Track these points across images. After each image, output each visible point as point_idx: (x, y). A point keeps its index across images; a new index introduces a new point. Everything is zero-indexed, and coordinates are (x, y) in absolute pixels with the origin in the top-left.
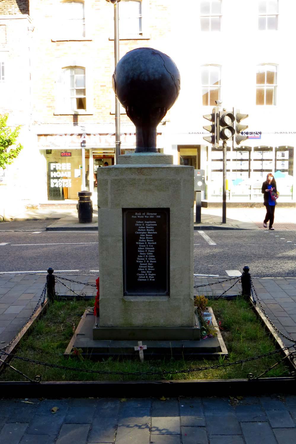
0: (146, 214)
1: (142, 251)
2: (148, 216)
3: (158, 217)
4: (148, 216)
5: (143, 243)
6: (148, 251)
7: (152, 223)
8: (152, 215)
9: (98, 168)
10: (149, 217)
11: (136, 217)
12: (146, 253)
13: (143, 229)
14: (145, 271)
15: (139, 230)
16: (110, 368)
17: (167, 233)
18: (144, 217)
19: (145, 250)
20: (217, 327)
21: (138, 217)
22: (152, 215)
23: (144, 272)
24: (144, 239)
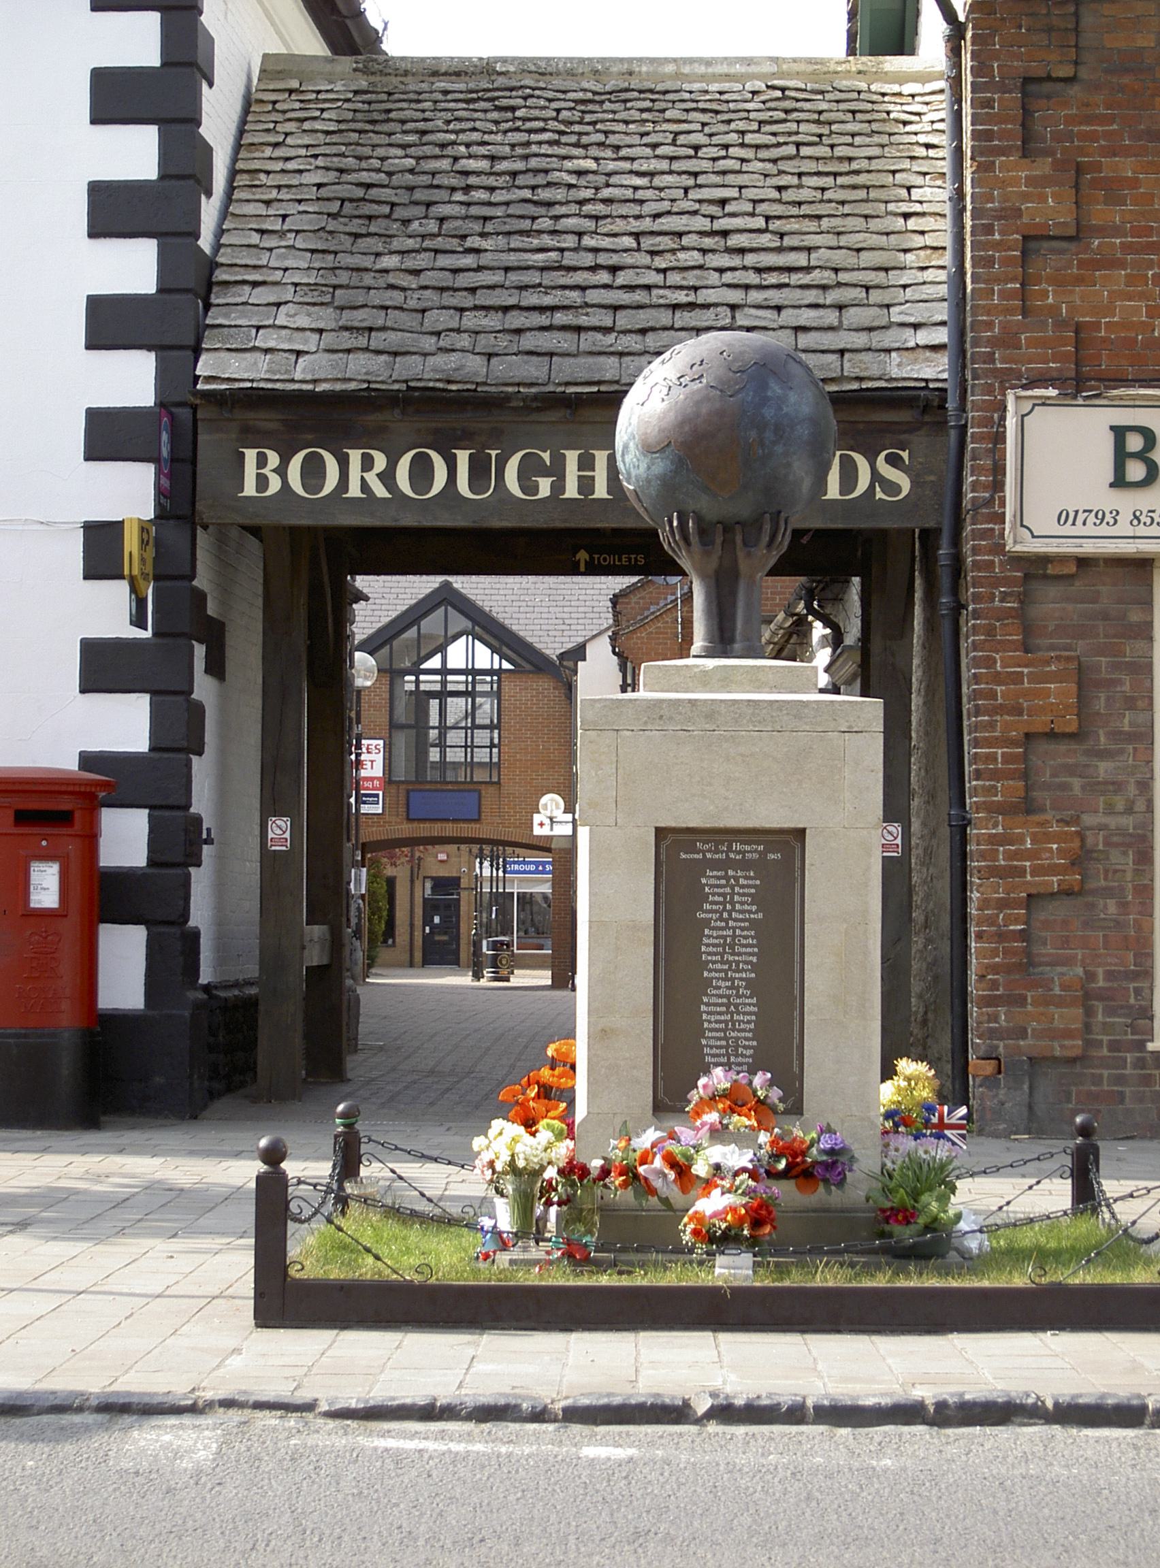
0: (730, 849)
1: (718, 1034)
2: (739, 852)
3: (771, 856)
4: (739, 852)
5: (724, 1009)
6: (737, 965)
7: (745, 954)
8: (746, 971)
9: (638, 1136)
10: (744, 856)
11: (700, 856)
12: (726, 921)
13: (717, 1047)
14: (721, 919)
15: (707, 906)
16: (551, 1173)
17: (796, 1028)
18: (727, 856)
19: (726, 1038)
20: (957, 1250)
21: (709, 856)
22: (752, 851)
23: (719, 966)
24: (727, 988)
